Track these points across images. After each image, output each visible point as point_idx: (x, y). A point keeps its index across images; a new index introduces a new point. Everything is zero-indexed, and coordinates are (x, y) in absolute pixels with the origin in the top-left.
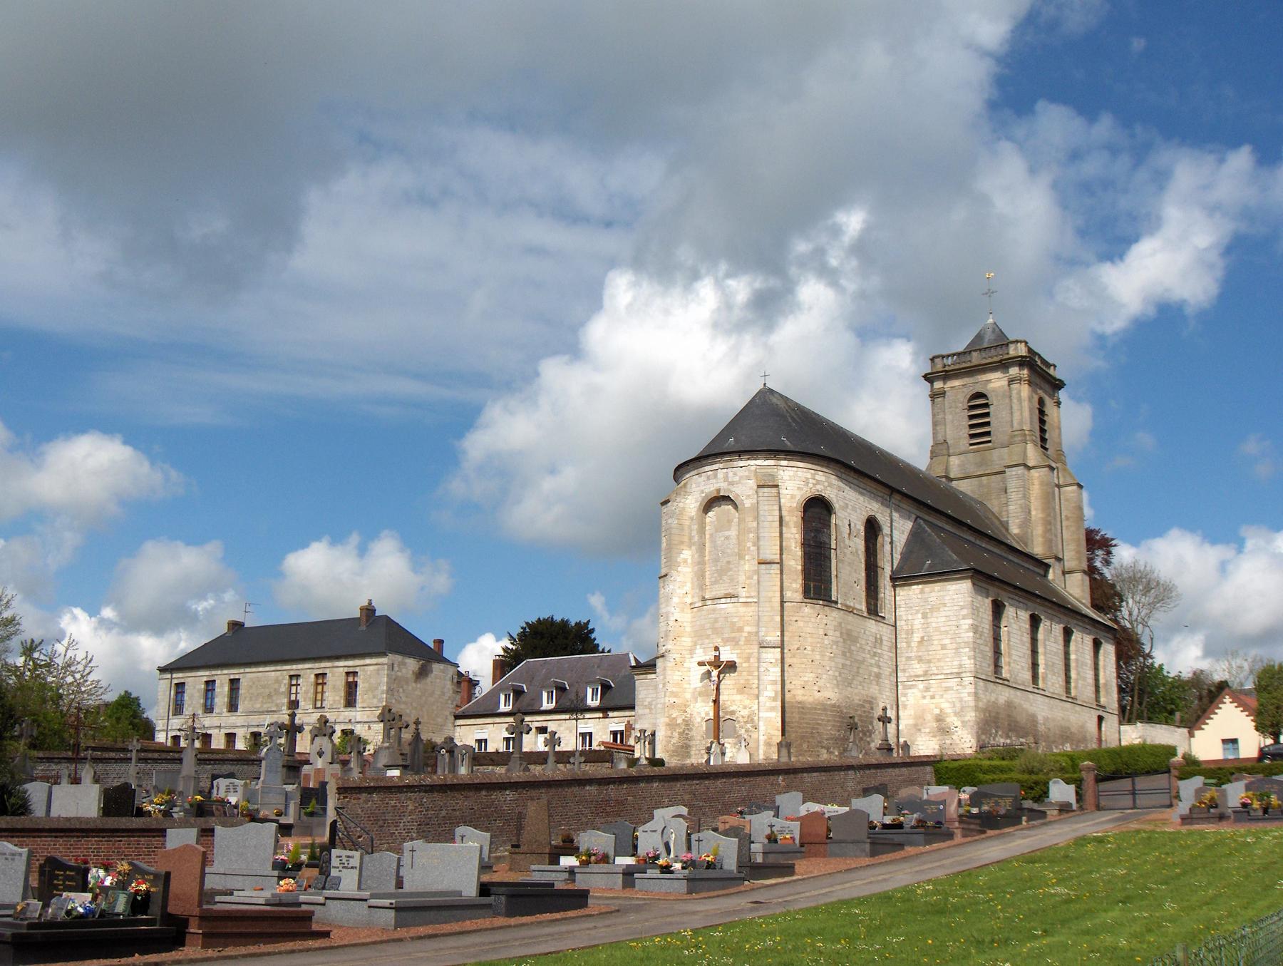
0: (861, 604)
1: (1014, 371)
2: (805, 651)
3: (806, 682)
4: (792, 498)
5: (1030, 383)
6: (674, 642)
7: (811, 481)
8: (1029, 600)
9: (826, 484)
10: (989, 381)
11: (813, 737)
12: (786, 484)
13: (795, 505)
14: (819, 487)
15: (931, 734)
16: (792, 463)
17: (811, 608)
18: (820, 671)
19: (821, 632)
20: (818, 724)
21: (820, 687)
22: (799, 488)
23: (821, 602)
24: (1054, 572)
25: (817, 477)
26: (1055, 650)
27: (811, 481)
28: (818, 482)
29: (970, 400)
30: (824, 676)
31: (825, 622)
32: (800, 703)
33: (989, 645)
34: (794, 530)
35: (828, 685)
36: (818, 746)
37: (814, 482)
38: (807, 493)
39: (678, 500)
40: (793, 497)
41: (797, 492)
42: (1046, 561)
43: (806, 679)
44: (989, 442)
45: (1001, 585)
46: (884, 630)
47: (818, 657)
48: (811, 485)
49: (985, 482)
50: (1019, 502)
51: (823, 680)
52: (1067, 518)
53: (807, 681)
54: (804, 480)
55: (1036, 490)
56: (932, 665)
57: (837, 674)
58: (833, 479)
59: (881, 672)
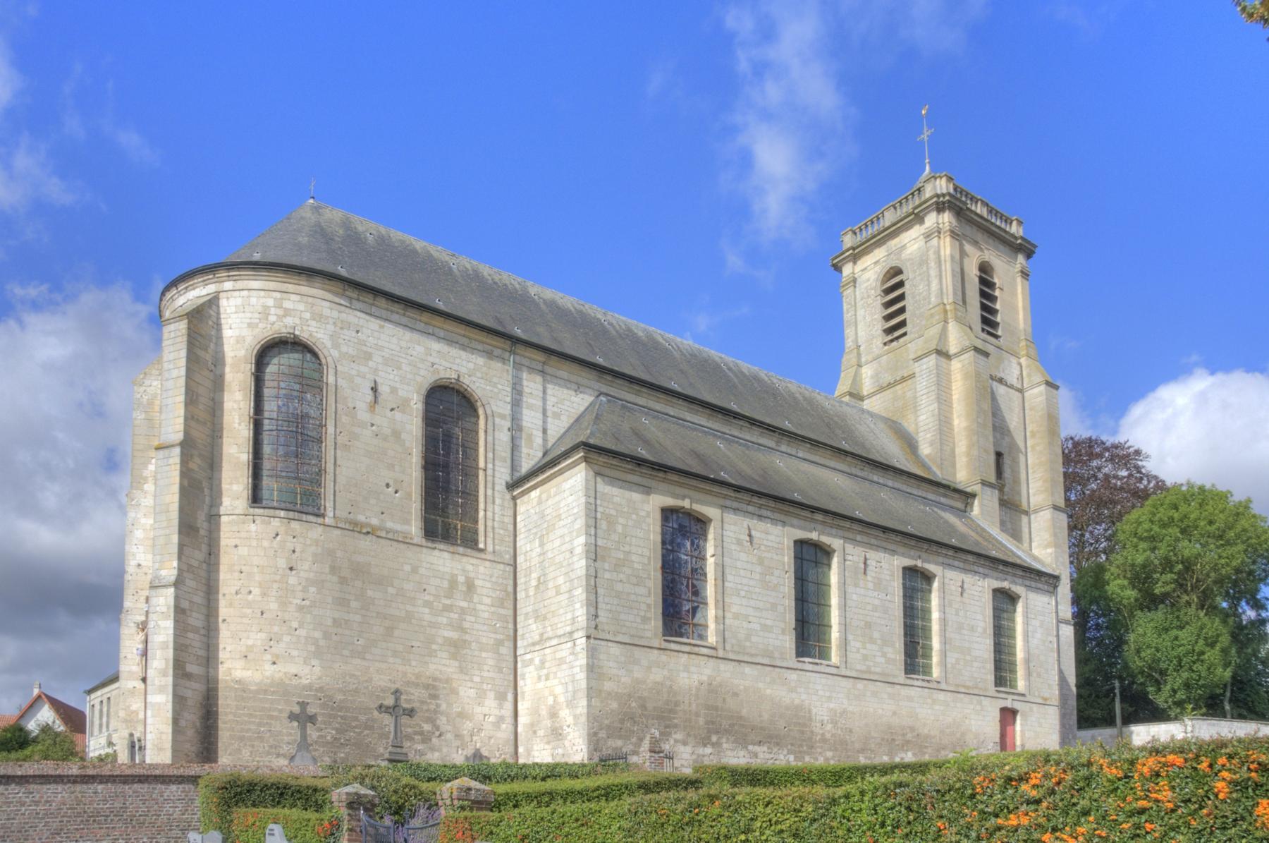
0: (408, 522)
1: (931, 219)
2: (250, 597)
3: (250, 648)
4: (238, 342)
5: (954, 234)
6: (136, 598)
7: (273, 311)
8: (787, 513)
9: (307, 315)
10: (904, 247)
11: (261, 739)
12: (230, 321)
13: (243, 353)
14: (289, 321)
15: (545, 740)
16: (240, 284)
17: (263, 522)
18: (276, 629)
19: (282, 563)
20: (272, 717)
21: (277, 656)
22: (250, 325)
23: (282, 513)
24: (981, 505)
25: (287, 304)
26: (877, 602)
27: (273, 311)
28: (287, 313)
29: (884, 282)
30: (287, 638)
31: (290, 546)
32: (239, 682)
33: (650, 584)
34: (239, 396)
35: (295, 653)
36: (269, 753)
37: (281, 312)
38: (426, 379)
39: (147, 382)
40: (240, 340)
41: (246, 332)
42: (969, 490)
43: (250, 642)
44: (905, 334)
45: (682, 480)
46: (481, 569)
47: (274, 606)
48: (272, 318)
49: (900, 392)
50: (931, 408)
51: (282, 645)
52: (1033, 435)
53: (252, 646)
54: (260, 309)
55: (959, 388)
56: (547, 623)
57: (318, 634)
58: (325, 308)
59: (467, 637)
